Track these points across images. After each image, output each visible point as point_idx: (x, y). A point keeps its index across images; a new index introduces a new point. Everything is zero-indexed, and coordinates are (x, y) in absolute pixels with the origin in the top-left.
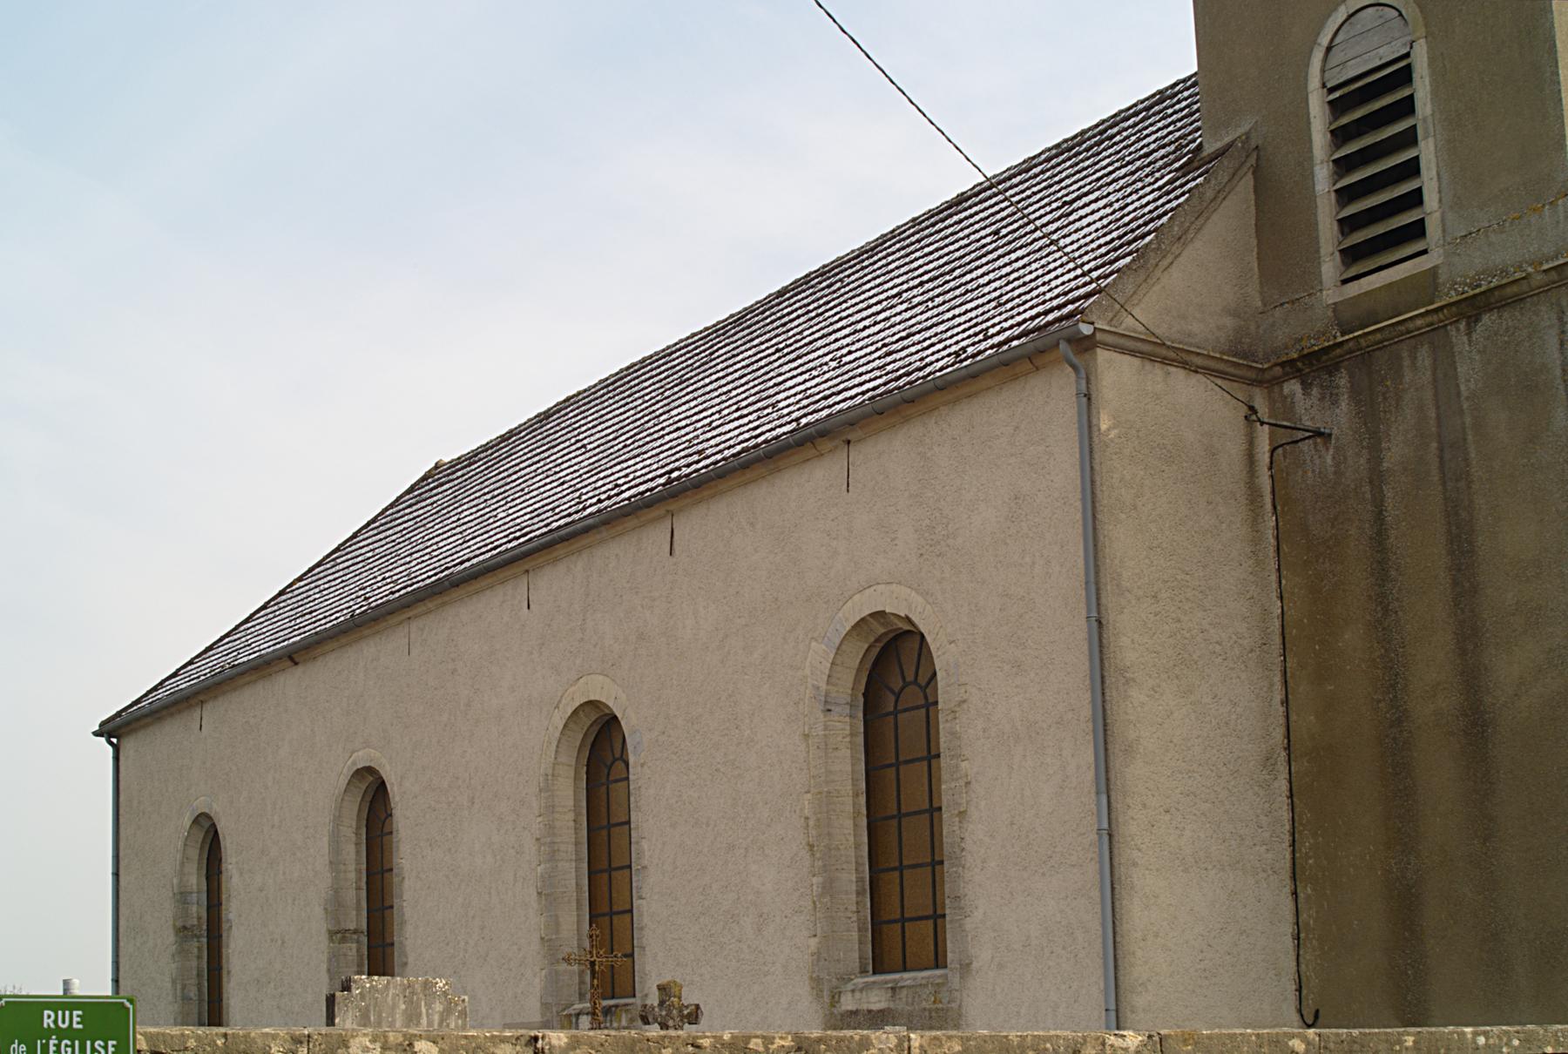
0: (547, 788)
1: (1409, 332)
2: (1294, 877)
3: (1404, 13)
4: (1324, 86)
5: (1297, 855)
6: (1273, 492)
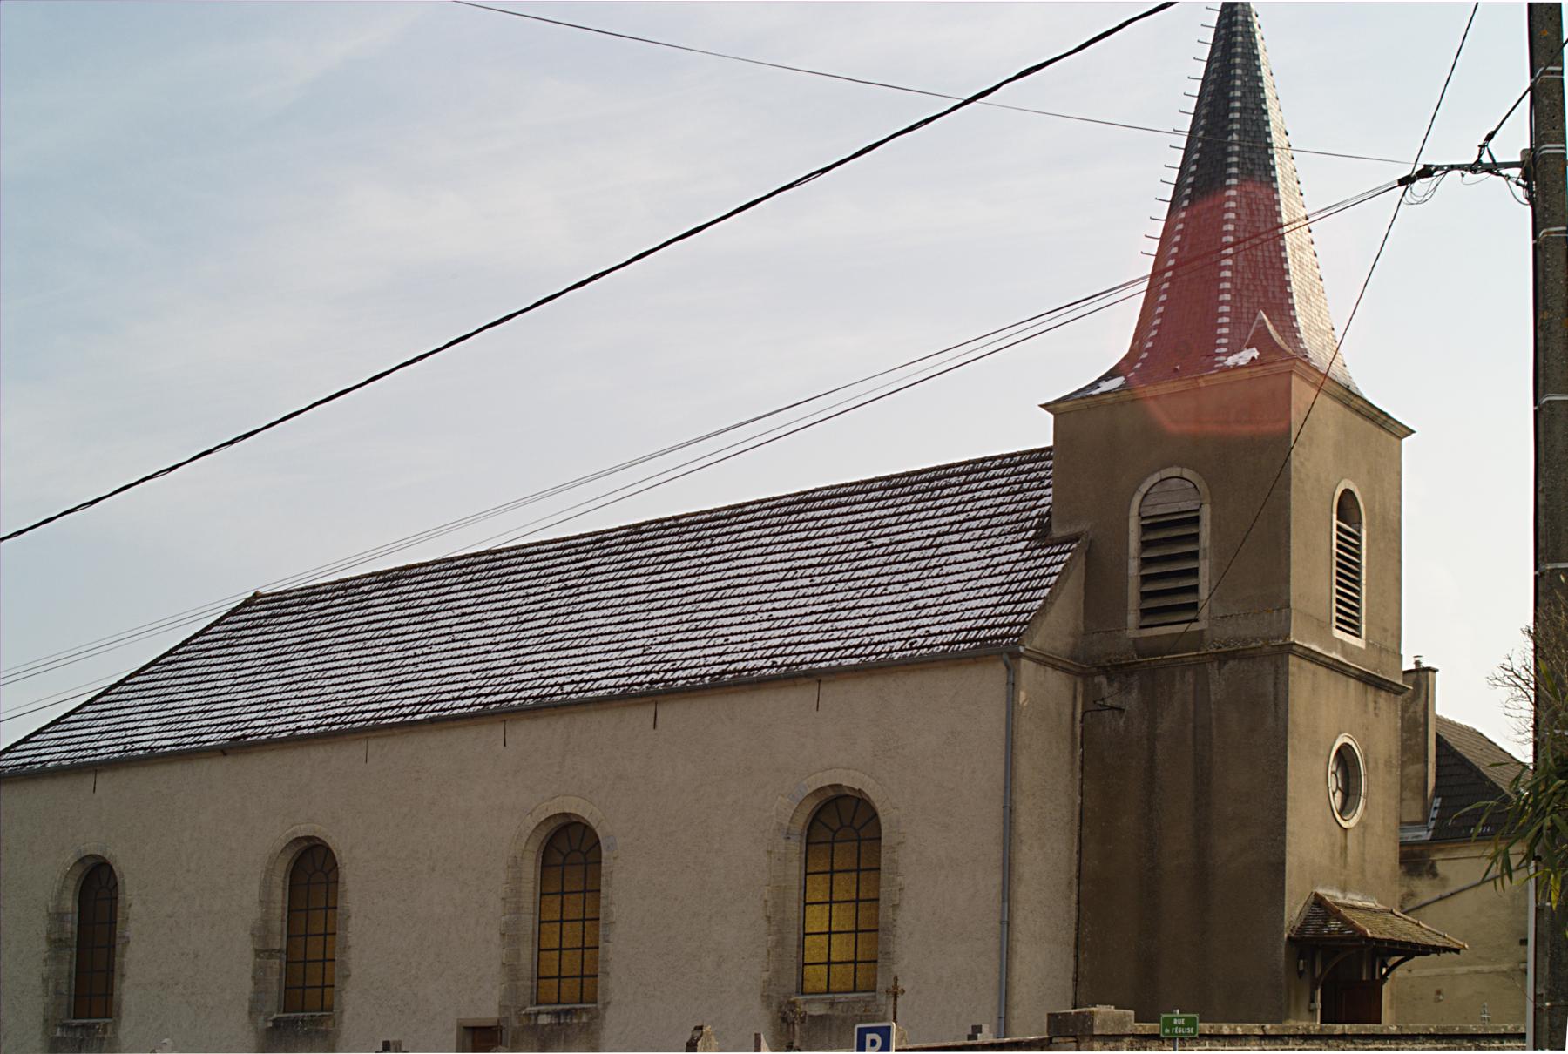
0: (515, 864)
2: (1077, 947)
4: (1139, 514)
6: (1082, 736)
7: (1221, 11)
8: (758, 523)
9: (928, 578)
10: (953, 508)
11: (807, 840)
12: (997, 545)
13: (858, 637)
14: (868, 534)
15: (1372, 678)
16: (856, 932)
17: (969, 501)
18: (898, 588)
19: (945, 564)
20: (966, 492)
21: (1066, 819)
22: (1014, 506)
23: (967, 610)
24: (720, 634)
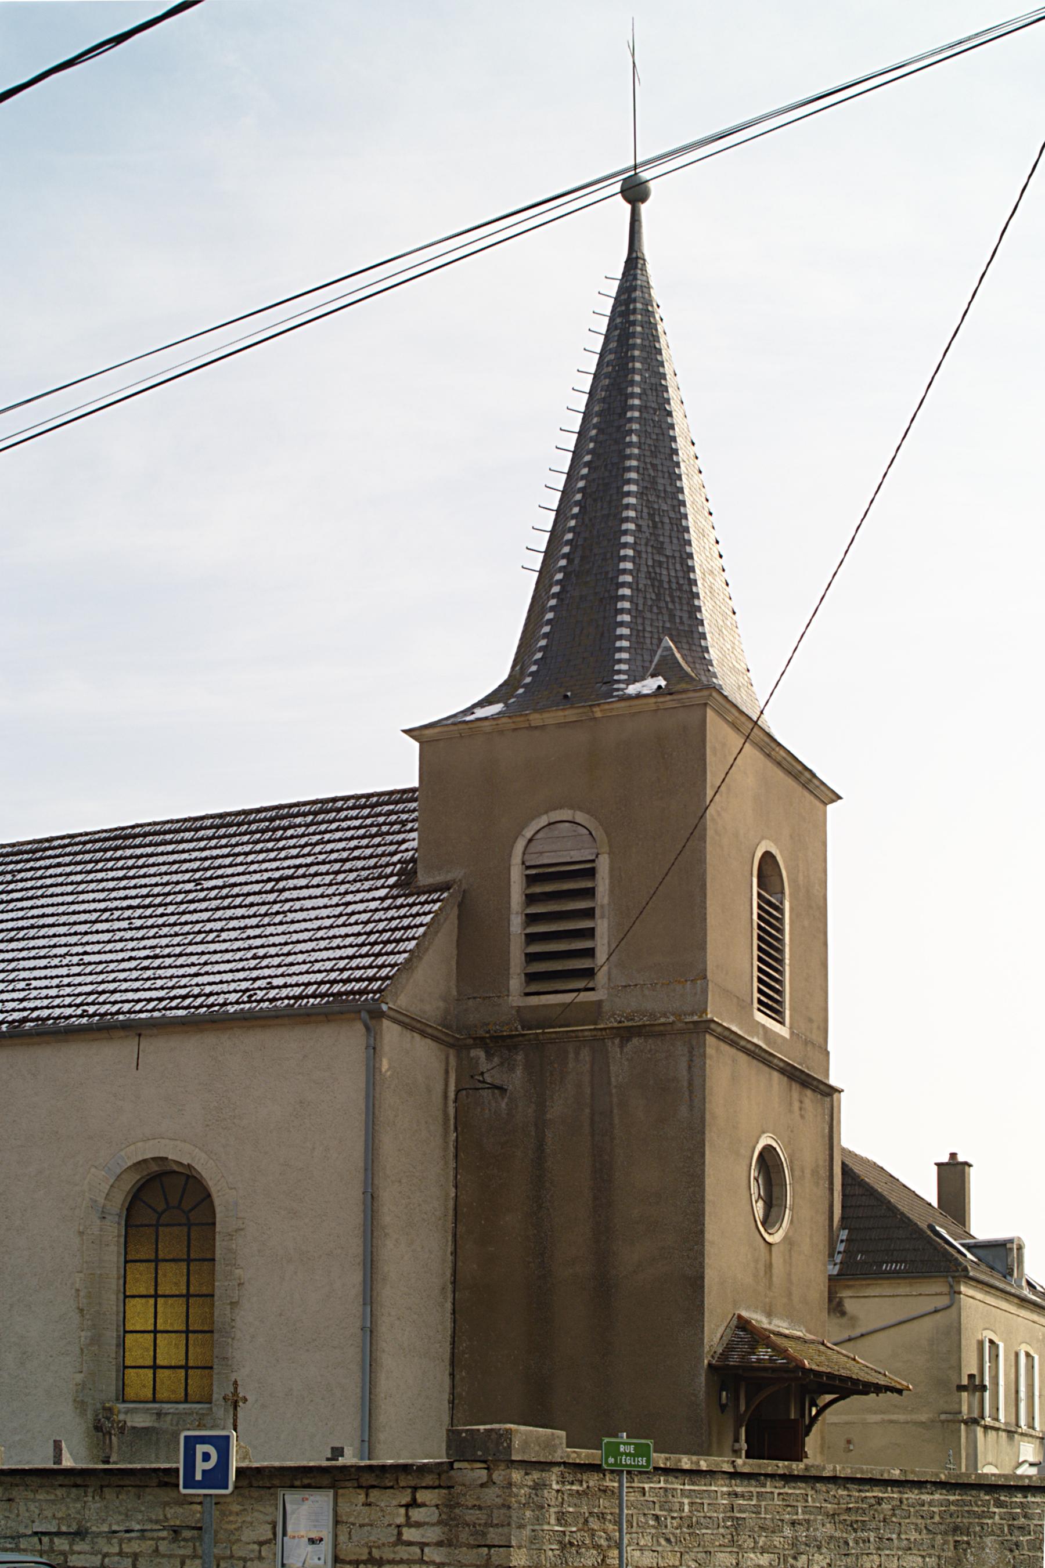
1: (576, 1037)
2: (452, 1363)
3: (594, 833)
4: (523, 863)
5: (456, 1351)
6: (456, 1118)
7: (616, 299)
8: (68, 859)
9: (269, 925)
10: (298, 850)
11: (126, 1221)
12: (352, 892)
13: (185, 986)
14: (198, 875)
15: (797, 1073)
16: (187, 1332)
17: (317, 844)
18: (233, 935)
19: (290, 911)
20: (314, 834)
21: (437, 1213)
22: (372, 850)
23: (317, 961)
24: (21, 977)
